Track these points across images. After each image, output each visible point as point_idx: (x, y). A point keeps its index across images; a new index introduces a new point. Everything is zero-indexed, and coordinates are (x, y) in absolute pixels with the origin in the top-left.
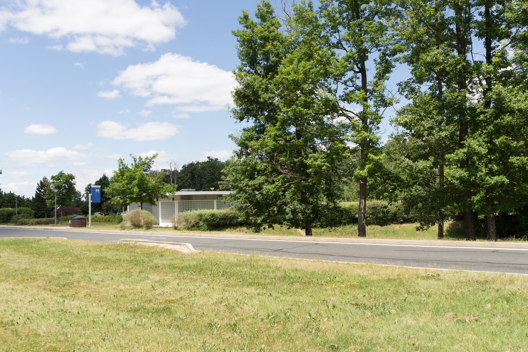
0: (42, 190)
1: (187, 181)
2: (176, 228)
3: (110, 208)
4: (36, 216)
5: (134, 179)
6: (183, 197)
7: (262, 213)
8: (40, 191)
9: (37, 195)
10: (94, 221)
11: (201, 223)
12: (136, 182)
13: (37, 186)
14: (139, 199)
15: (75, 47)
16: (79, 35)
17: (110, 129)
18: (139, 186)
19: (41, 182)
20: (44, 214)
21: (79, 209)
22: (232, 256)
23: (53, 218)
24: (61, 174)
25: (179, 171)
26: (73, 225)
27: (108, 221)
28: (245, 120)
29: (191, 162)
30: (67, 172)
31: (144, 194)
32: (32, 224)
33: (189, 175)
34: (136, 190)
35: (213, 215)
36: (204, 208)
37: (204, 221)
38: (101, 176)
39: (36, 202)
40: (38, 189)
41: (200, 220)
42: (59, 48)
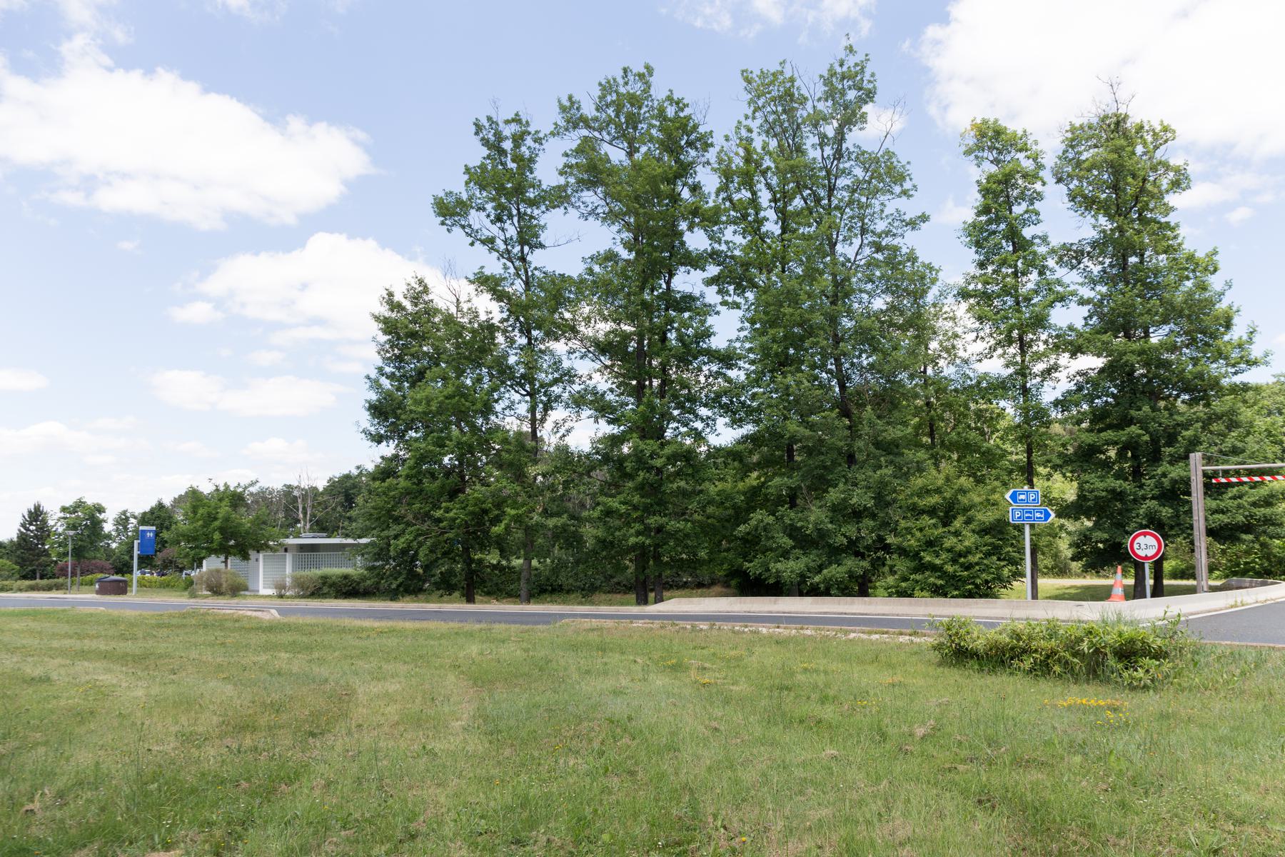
0: (32, 528)
1: (334, 509)
2: (281, 596)
3: (171, 562)
4: (24, 577)
5: (215, 519)
6: (302, 548)
7: (399, 577)
8: (28, 529)
9: (22, 537)
10: (141, 584)
11: (326, 590)
12: (217, 523)
13: (21, 520)
14: (223, 550)
15: (112, 199)
16: (125, 176)
17: (183, 386)
18: (222, 530)
19: (30, 512)
20: (34, 572)
21: (108, 565)
22: (310, 620)
23: (127, 577)
24: (79, 505)
25: (321, 489)
26: (102, 591)
27: (166, 586)
28: (384, 443)
29: (346, 472)
30: (90, 500)
31: (232, 542)
32: (20, 590)
33: (341, 498)
34: (217, 536)
35: (346, 577)
36: (330, 566)
37: (330, 586)
38: (154, 503)
39: (17, 549)
40: (23, 525)
41: (324, 584)
42: (73, 199)
